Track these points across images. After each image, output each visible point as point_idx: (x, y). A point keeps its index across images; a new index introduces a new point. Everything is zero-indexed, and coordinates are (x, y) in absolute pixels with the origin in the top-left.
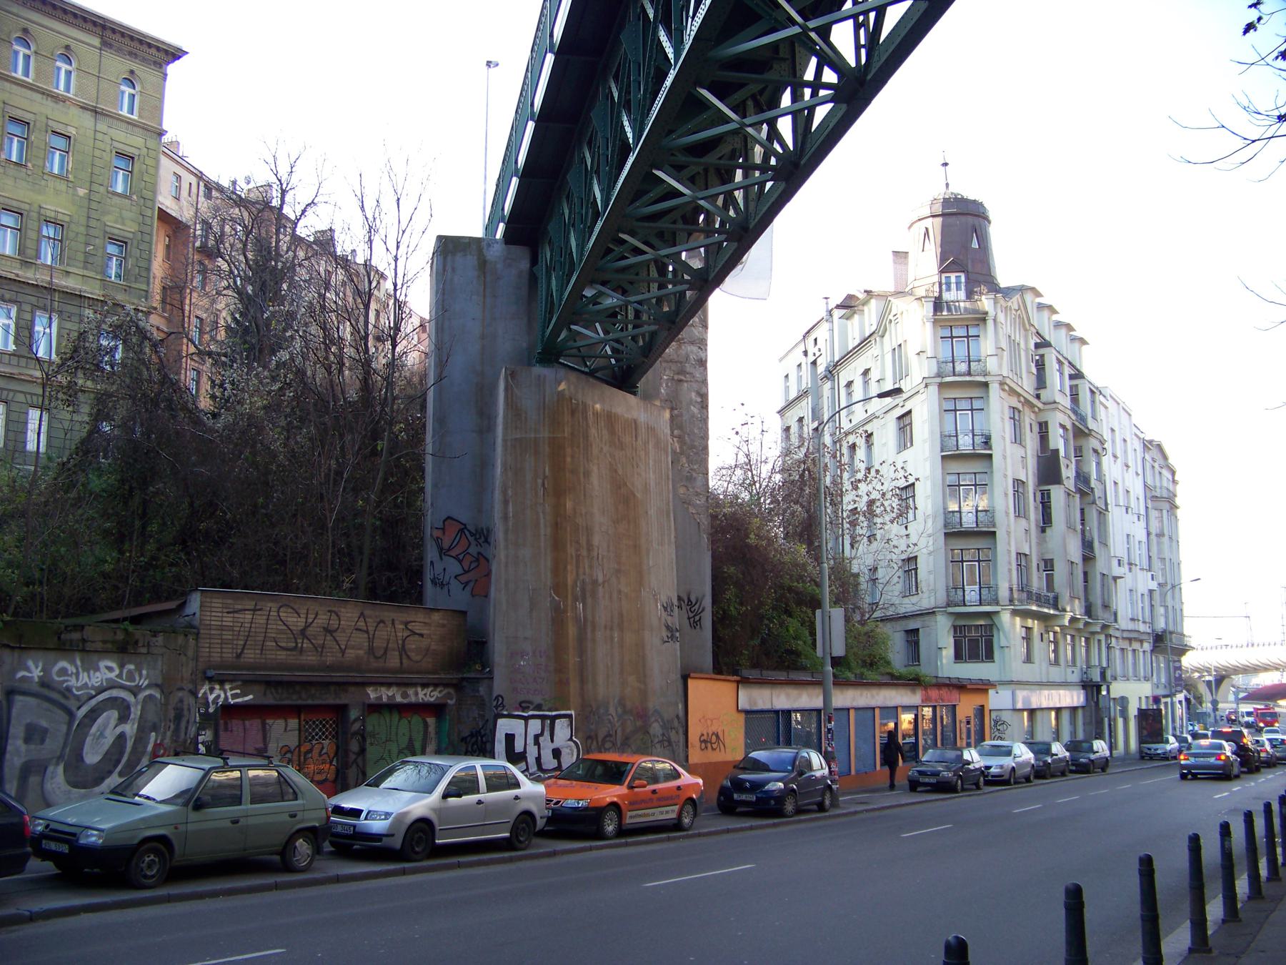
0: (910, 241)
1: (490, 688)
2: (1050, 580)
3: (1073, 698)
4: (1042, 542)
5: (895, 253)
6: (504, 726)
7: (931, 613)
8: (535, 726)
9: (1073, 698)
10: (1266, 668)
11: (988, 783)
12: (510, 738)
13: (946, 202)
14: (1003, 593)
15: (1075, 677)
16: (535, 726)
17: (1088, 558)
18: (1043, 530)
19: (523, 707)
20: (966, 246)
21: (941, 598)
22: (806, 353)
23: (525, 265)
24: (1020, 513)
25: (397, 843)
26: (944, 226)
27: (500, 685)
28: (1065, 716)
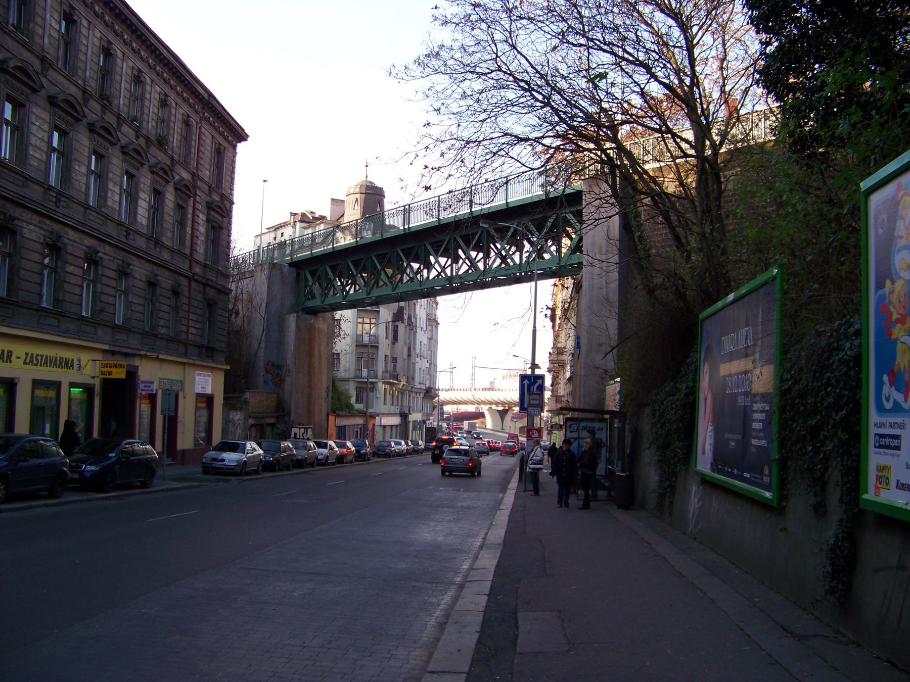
0: (350, 202)
1: (289, 418)
2: (395, 366)
3: (396, 420)
4: (392, 349)
5: (332, 199)
6: (294, 430)
7: (348, 380)
8: (302, 430)
9: (396, 420)
10: (466, 403)
11: (319, 464)
12: (295, 434)
13: (368, 187)
14: (380, 373)
15: (398, 411)
16: (302, 430)
17: (409, 356)
18: (393, 344)
19: (299, 424)
20: (374, 210)
21: (352, 375)
22: (275, 239)
23: (295, 275)
24: (387, 337)
25: (239, 469)
26: (365, 199)
27: (293, 417)
28: (388, 429)
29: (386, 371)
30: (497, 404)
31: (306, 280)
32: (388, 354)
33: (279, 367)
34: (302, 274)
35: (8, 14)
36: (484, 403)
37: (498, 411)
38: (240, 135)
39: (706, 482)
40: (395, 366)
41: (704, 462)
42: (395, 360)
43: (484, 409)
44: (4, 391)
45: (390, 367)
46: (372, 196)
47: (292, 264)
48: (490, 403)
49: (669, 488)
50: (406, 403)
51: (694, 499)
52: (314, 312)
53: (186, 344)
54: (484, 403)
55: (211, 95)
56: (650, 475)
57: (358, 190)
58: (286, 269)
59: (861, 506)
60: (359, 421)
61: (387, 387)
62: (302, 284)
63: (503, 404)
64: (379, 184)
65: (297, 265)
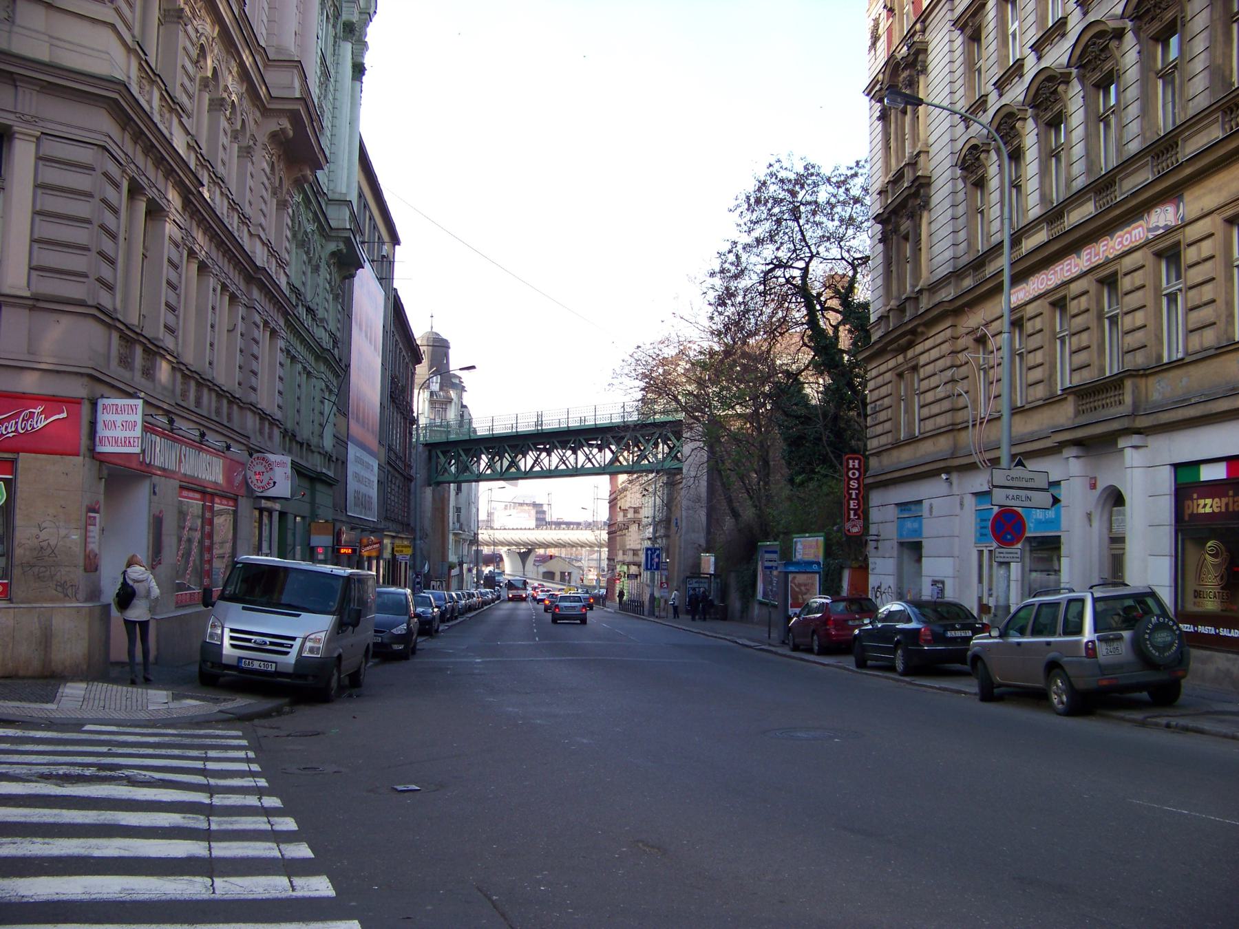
6: (433, 583)
30: (517, 544)
31: (438, 457)
34: (433, 453)
36: (502, 544)
37: (519, 553)
39: (761, 603)
41: (760, 597)
43: (503, 550)
46: (540, 416)
47: (427, 445)
48: (509, 544)
49: (745, 609)
51: (756, 610)
52: (439, 484)
54: (502, 544)
56: (735, 603)
59: (878, 106)
62: (434, 461)
63: (525, 544)
64: (444, 337)
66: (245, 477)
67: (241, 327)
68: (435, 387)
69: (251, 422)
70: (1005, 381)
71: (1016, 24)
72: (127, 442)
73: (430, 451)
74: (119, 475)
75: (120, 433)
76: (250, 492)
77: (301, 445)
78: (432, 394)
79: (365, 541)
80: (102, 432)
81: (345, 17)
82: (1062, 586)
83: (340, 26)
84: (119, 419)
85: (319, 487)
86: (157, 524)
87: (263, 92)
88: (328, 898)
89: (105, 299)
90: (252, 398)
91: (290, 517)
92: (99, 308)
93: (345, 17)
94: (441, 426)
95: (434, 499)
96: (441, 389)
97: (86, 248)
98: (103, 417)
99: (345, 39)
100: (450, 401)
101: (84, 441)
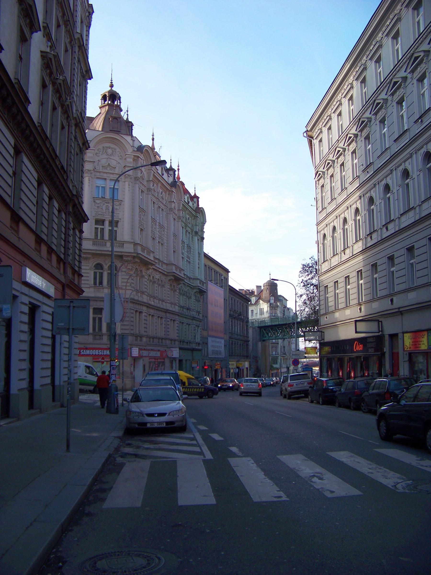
2: (284, 350)
5: (257, 286)
6: (262, 375)
14: (280, 353)
29: (281, 352)
32: (282, 345)
33: (256, 357)
35: (140, 221)
38: (91, 78)
40: (284, 350)
42: (284, 347)
44: (29, 328)
45: (283, 351)
50: (288, 363)
53: (244, 356)
55: (221, 265)
57: (267, 285)
58: (257, 328)
60: (276, 371)
61: (282, 358)
65: (260, 328)
66: (167, 354)
67: (164, 323)
68: (272, 301)
69: (168, 342)
70: (236, 341)
71: (356, 160)
72: (136, 354)
73: (260, 329)
74: (135, 359)
75: (135, 353)
76: (168, 357)
77: (187, 343)
78: (270, 304)
79: (216, 364)
80: (132, 353)
81: (195, 230)
82: (118, 389)
83: (194, 233)
84: (135, 351)
85: (194, 352)
86: (144, 366)
87: (166, 273)
88: (211, 460)
89: (132, 332)
90: (168, 337)
91: (184, 361)
92: (131, 334)
93: (195, 230)
94: (274, 316)
95: (262, 346)
96: (275, 302)
97: (128, 325)
98: (132, 351)
99: (195, 236)
100: (278, 306)
101: (130, 355)
